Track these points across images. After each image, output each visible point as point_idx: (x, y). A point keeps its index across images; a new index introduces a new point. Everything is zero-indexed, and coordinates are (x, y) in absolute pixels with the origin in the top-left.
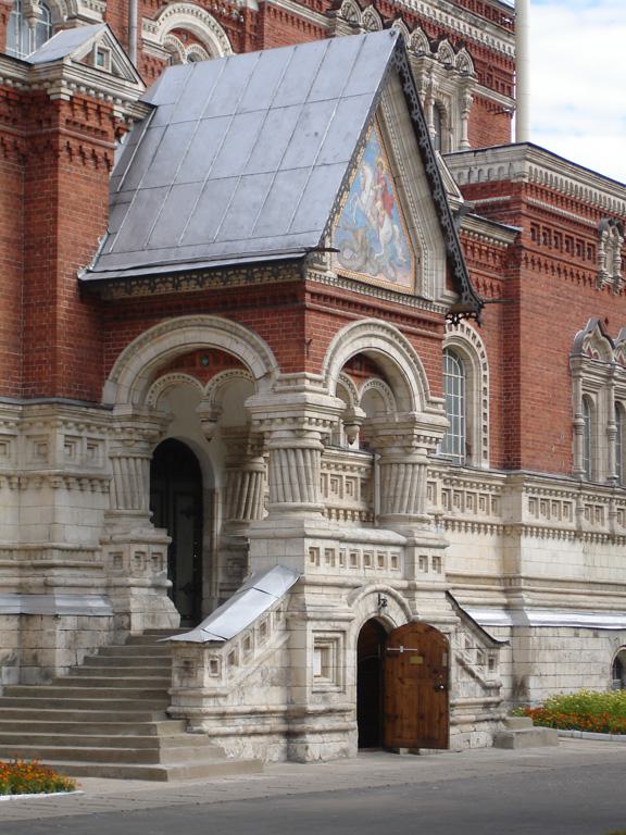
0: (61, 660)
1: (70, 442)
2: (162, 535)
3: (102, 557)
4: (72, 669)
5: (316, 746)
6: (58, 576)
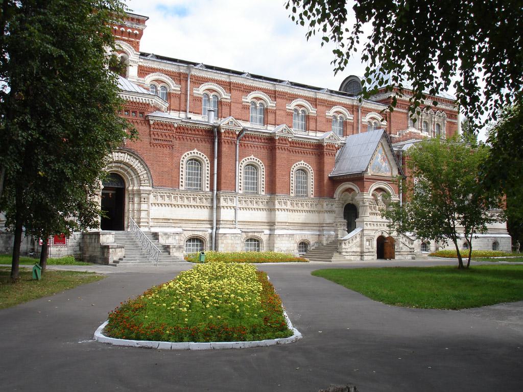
0: (325, 243)
1: (327, 205)
2: (346, 221)
3: (334, 225)
4: (328, 244)
5: (366, 258)
6: (324, 228)
